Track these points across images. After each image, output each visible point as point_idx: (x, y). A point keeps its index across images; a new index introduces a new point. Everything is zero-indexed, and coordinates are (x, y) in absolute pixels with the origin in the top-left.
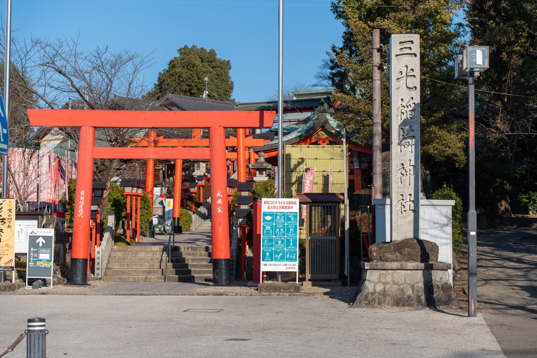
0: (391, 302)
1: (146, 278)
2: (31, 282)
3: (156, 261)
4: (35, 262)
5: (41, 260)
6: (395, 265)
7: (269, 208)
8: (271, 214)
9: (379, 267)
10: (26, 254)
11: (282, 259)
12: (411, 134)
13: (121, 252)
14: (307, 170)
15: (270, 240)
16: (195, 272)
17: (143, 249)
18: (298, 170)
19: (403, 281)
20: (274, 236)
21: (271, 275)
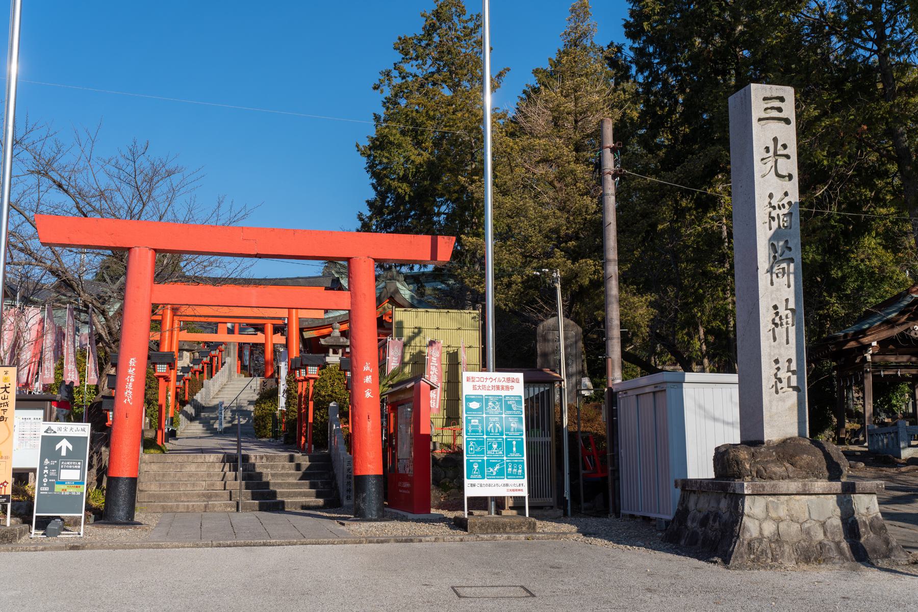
0: (793, 556)
1: (206, 506)
2: (43, 524)
3: (215, 478)
4: (51, 486)
5: (63, 482)
6: (794, 486)
7: (474, 388)
8: (478, 399)
9: (768, 490)
10: (34, 470)
11: (500, 474)
12: (788, 254)
13: (158, 465)
14: (432, 343)
15: (480, 443)
16: (282, 494)
17: (190, 459)
18: (413, 343)
19: (807, 515)
20: (485, 437)
21: (479, 503)
